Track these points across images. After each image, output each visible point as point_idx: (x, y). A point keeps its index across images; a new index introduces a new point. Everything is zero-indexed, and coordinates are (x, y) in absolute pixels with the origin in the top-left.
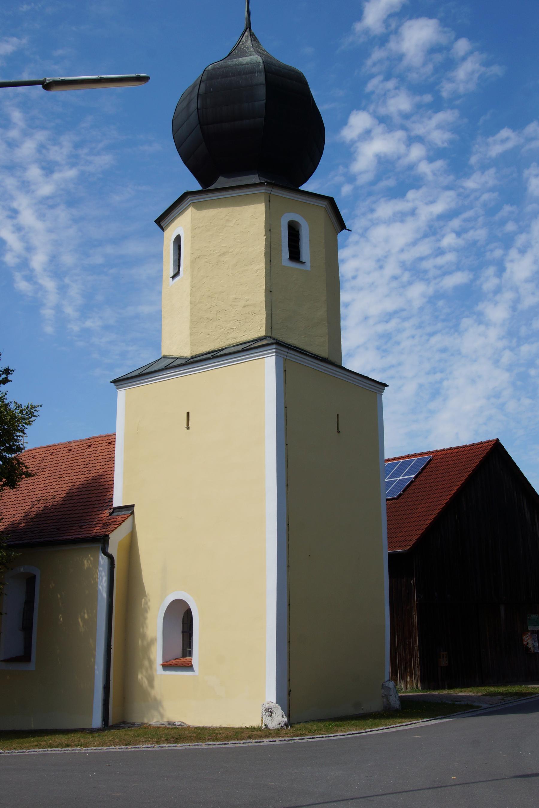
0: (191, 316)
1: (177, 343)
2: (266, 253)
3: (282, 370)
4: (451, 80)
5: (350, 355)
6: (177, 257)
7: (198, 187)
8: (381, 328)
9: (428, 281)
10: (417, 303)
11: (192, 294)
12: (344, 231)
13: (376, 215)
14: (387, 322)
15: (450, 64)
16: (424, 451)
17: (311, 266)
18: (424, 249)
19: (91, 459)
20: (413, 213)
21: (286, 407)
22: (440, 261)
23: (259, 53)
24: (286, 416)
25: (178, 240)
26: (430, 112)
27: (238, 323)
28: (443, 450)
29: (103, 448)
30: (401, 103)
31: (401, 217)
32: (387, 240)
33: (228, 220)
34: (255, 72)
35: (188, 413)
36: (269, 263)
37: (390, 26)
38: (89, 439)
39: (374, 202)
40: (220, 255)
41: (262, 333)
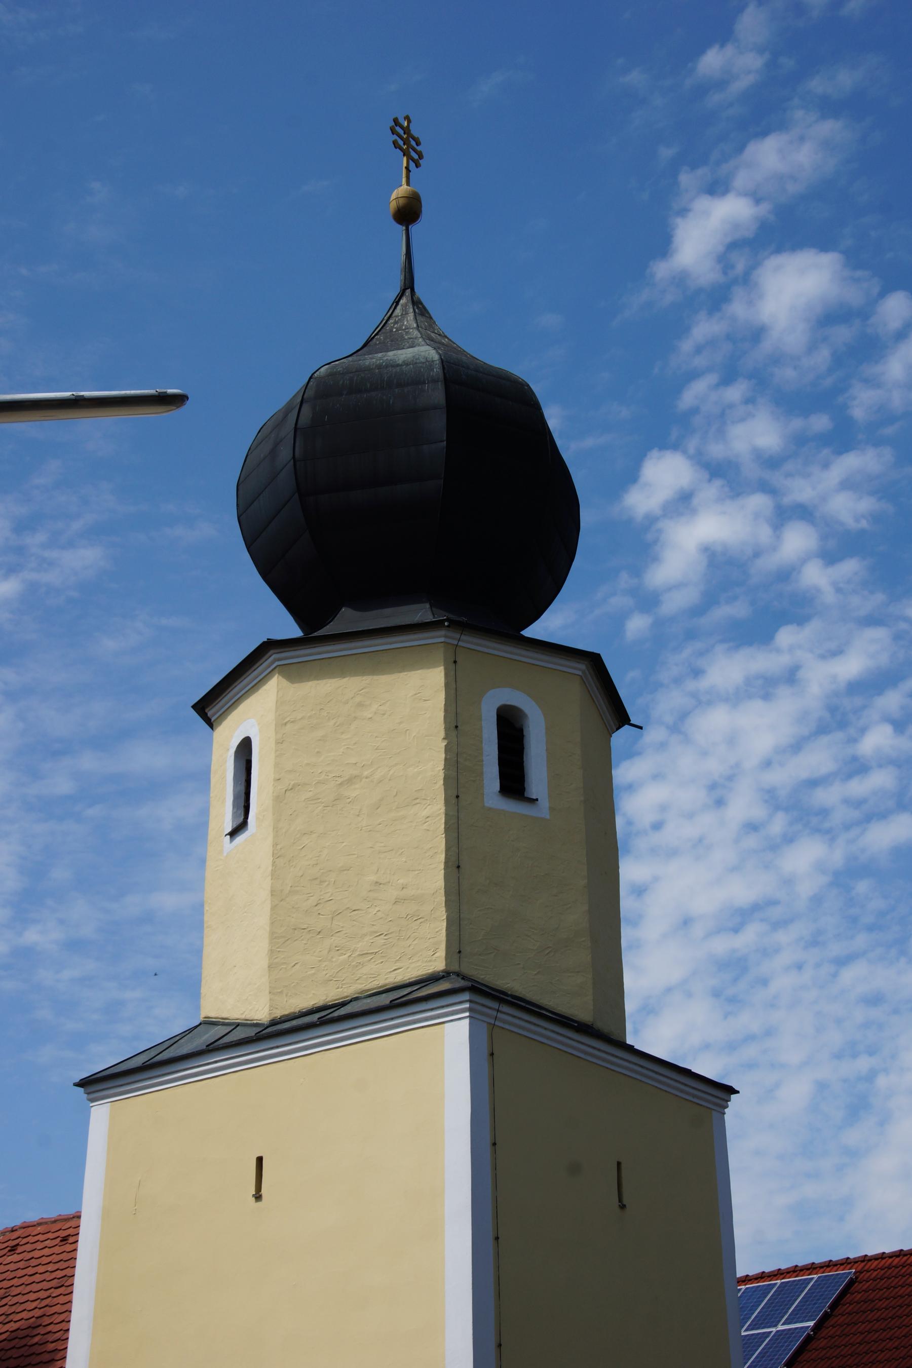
0: (272, 923)
1: (238, 989)
2: (446, 779)
3: (485, 1052)
4: (873, 382)
5: (650, 1009)
6: (242, 788)
7: (290, 629)
8: (721, 945)
9: (830, 835)
10: (806, 889)
11: (274, 875)
12: (627, 726)
13: (704, 683)
14: (736, 930)
15: (869, 348)
16: (835, 1258)
17: (552, 809)
18: (819, 759)
19: (15, 1282)
20: (791, 677)
21: (494, 1144)
22: (858, 787)
23: (432, 340)
24: (495, 1168)
25: (245, 747)
26: (826, 452)
27: (381, 940)
28: (882, 1256)
29: (47, 1252)
30: (759, 433)
31: (764, 687)
32: (732, 740)
33: (360, 705)
34: (425, 383)
35: (260, 1160)
36: (454, 800)
37: (733, 267)
38: (13, 1230)
39: (701, 654)
40: (341, 784)
41: (438, 964)
